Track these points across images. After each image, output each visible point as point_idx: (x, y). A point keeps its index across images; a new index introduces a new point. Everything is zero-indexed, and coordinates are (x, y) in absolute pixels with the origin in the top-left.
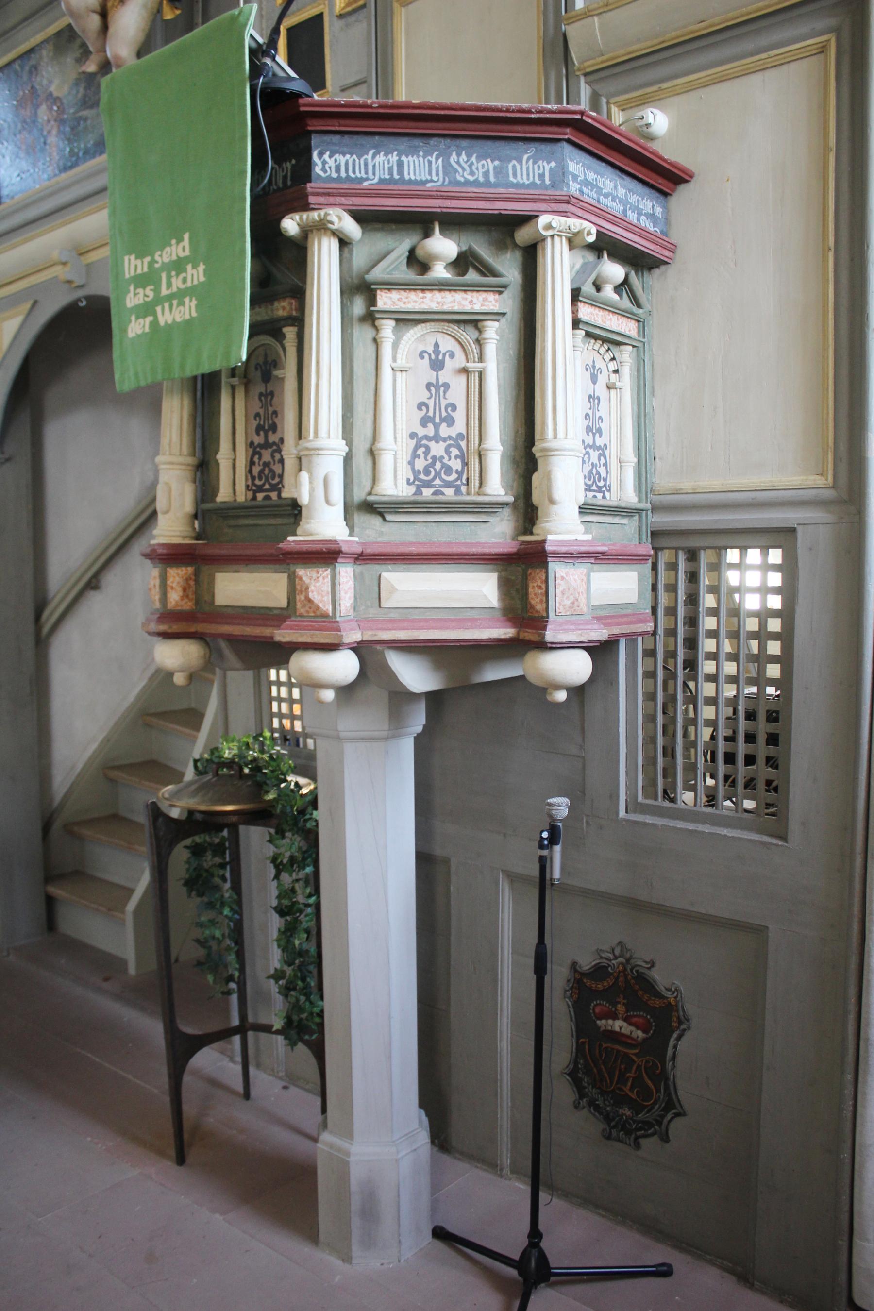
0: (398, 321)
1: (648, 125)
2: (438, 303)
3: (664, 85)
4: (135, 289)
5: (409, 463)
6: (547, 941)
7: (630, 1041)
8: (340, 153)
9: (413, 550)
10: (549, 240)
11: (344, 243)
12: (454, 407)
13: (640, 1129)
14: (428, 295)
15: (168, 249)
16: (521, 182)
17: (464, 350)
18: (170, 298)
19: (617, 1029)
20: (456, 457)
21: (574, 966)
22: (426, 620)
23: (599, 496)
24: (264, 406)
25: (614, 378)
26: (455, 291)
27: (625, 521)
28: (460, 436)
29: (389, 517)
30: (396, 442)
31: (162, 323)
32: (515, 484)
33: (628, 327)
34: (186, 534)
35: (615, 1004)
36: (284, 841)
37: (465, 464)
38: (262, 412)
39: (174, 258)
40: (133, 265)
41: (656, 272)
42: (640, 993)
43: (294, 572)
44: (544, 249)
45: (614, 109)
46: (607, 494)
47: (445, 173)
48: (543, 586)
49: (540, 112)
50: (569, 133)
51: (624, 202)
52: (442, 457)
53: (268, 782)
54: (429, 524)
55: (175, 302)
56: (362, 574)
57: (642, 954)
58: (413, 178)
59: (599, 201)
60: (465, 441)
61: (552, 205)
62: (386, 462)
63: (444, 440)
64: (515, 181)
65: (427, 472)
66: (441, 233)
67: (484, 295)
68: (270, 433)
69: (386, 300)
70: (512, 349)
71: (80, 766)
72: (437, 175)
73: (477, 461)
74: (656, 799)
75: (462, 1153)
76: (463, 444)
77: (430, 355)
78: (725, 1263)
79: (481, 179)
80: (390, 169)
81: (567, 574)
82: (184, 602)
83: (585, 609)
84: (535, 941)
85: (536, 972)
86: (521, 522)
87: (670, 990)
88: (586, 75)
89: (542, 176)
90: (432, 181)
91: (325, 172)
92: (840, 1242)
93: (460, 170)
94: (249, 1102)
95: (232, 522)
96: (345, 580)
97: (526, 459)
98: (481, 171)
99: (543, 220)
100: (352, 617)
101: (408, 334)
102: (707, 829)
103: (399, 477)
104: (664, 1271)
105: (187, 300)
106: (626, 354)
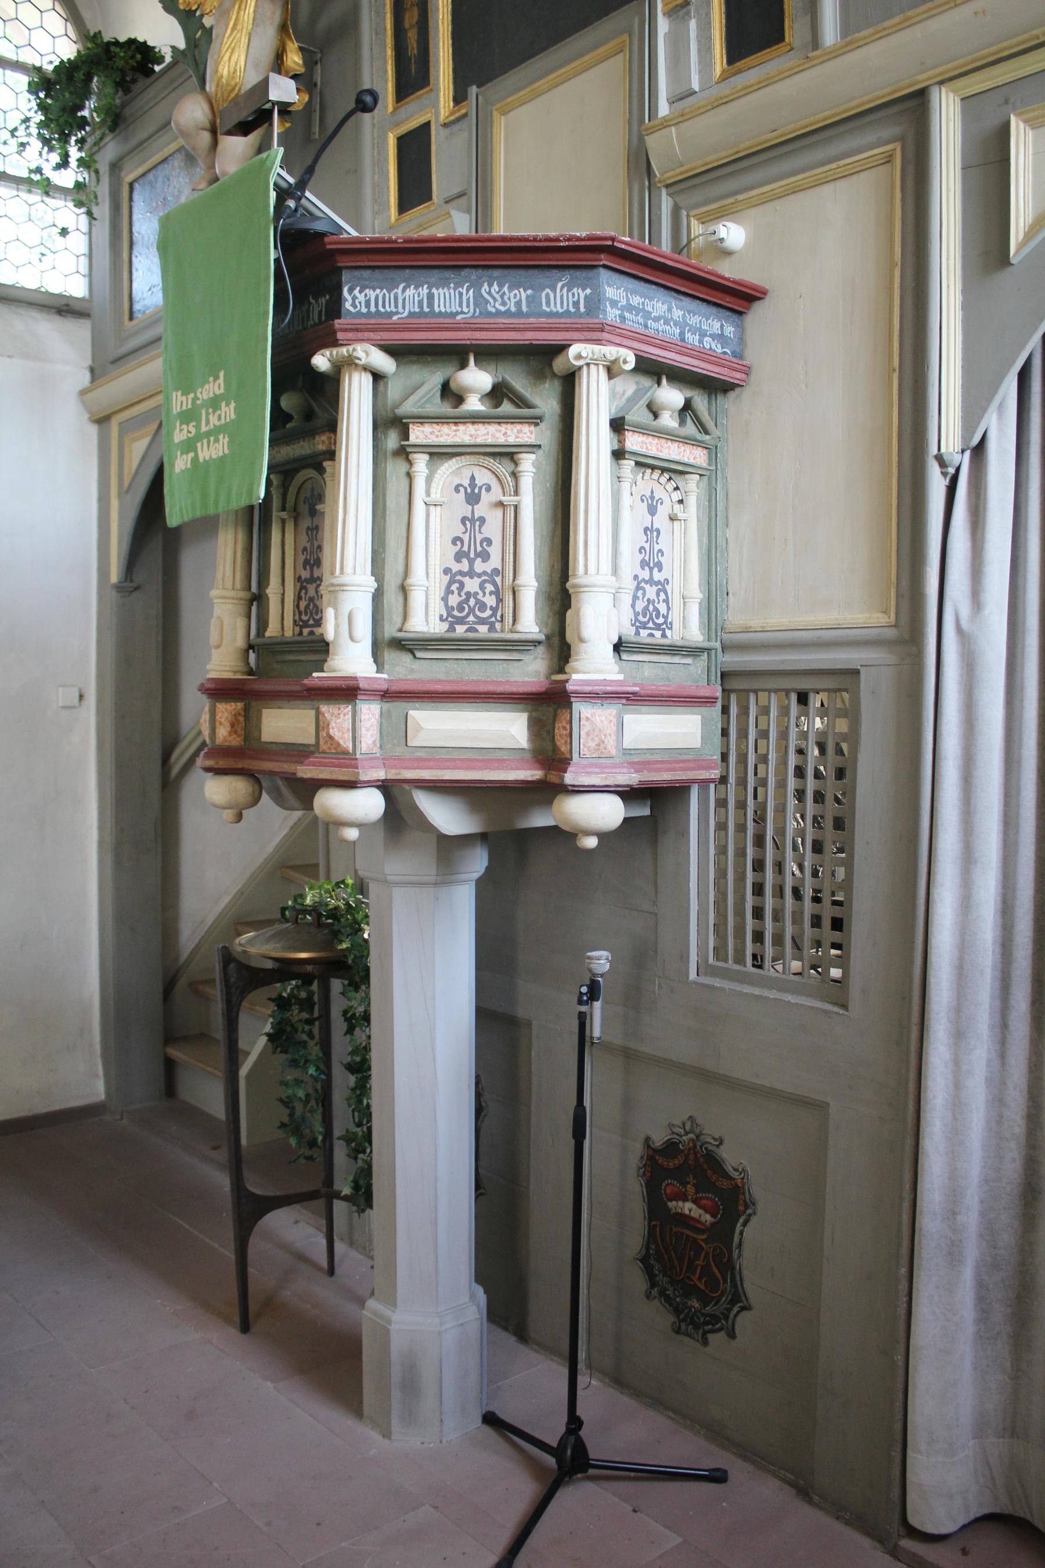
0: (431, 454)
1: (722, 240)
2: (471, 436)
3: (741, 197)
4: (181, 424)
5: (442, 599)
6: (587, 1103)
7: (698, 1225)
8: (370, 288)
9: (439, 687)
10: (585, 368)
11: (377, 377)
12: (489, 542)
13: (706, 1323)
14: (461, 427)
15: (207, 386)
16: (555, 310)
17: (499, 480)
18: (208, 434)
19: (687, 1212)
20: (491, 593)
21: (648, 1139)
22: (454, 760)
23: (658, 634)
24: (311, 540)
25: (678, 508)
26: (488, 423)
27: (689, 660)
28: (495, 571)
29: (419, 654)
30: (428, 577)
31: (201, 460)
32: (550, 621)
33: (696, 456)
34: (237, 669)
35: (684, 1184)
36: (357, 995)
37: (500, 600)
38: (308, 546)
39: (211, 395)
40: (179, 402)
41: (732, 395)
42: (709, 1172)
44: (580, 378)
45: (694, 222)
46: (668, 633)
47: (476, 305)
48: (568, 727)
49: (569, 240)
50: (604, 259)
51: (682, 325)
52: (476, 593)
53: (343, 930)
54: (461, 662)
55: (212, 439)
56: (389, 711)
57: (711, 1129)
58: (443, 310)
59: (646, 326)
60: (500, 577)
61: (585, 333)
62: (417, 598)
63: (479, 576)
64: (548, 310)
65: (461, 608)
66: (476, 364)
67: (519, 427)
68: (315, 568)
69: (419, 434)
70: (549, 482)
71: (209, 922)
72: (468, 306)
73: (511, 597)
74: (726, 961)
75: (538, 1344)
76: (498, 580)
77: (466, 489)
78: (789, 1475)
79: (513, 309)
80: (421, 302)
81: (593, 715)
82: (231, 738)
83: (614, 752)
84: (574, 1102)
85: (574, 1137)
86: (556, 660)
87: (736, 1170)
88: (667, 186)
89: (576, 304)
90: (462, 313)
91: (355, 307)
92: (893, 1453)
93: (491, 301)
94: (332, 1279)
95: (279, 658)
96: (367, 717)
97: (560, 598)
98: (513, 300)
99: (573, 350)
100: (378, 755)
101: (443, 468)
102: (773, 994)
103: (431, 613)
104: (718, 1477)
105: (221, 437)
106: (692, 483)
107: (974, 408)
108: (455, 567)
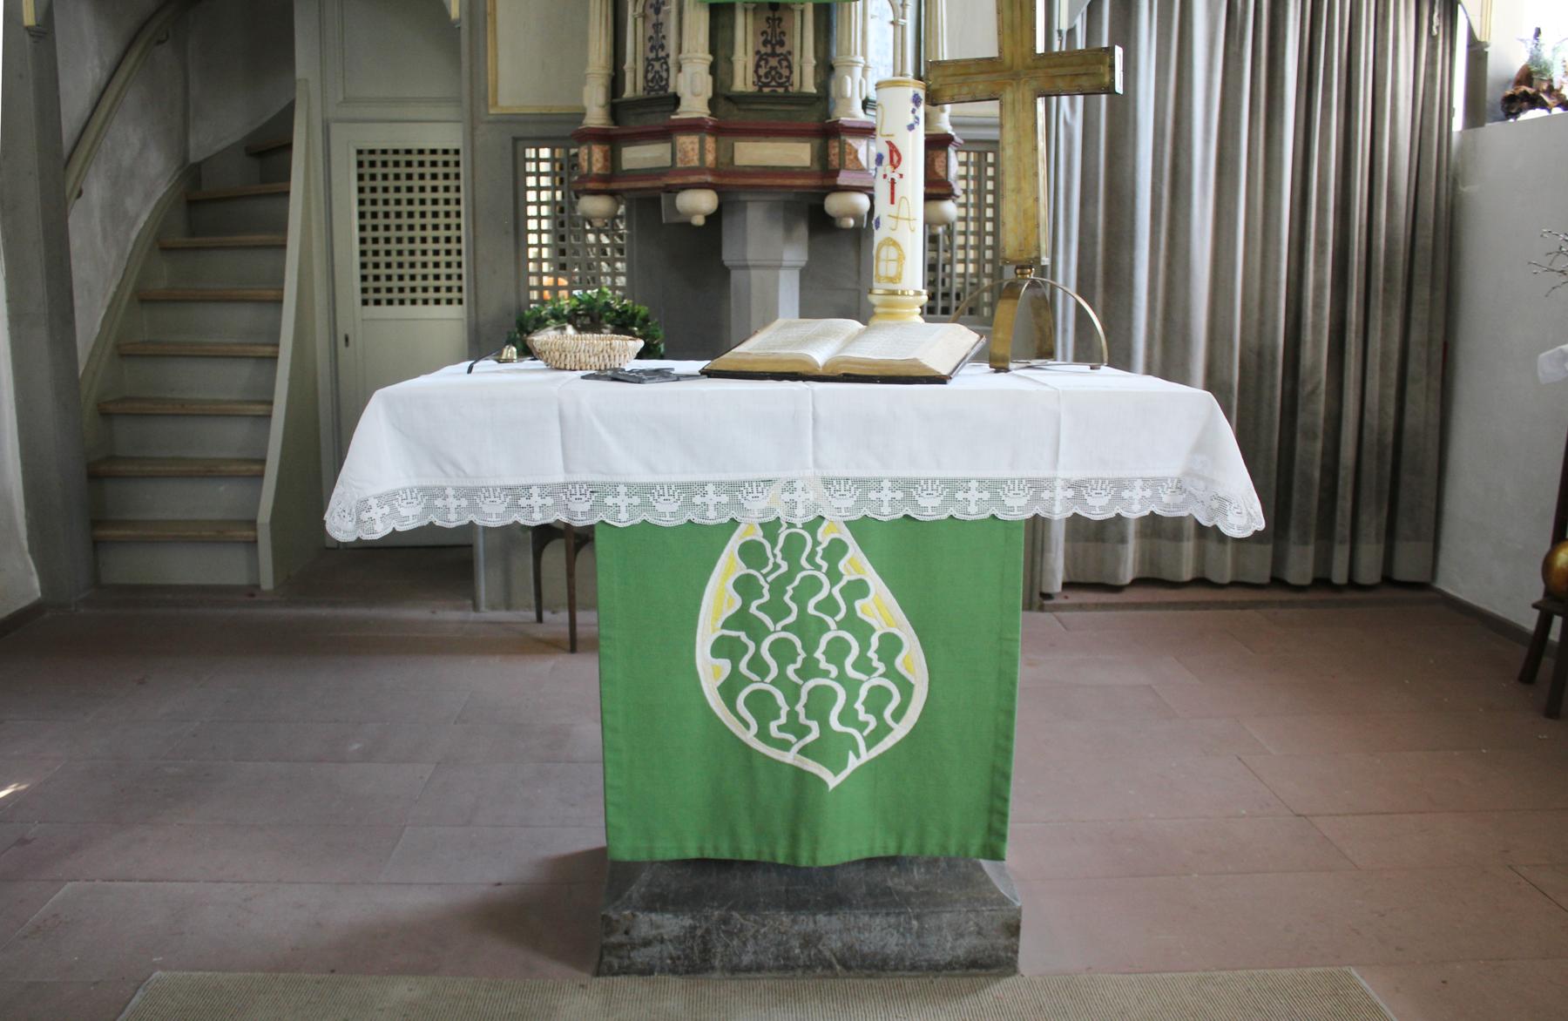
24: (657, 32)
43: (845, 143)
65: (766, 76)
107: (1072, 17)
108: (763, 50)
